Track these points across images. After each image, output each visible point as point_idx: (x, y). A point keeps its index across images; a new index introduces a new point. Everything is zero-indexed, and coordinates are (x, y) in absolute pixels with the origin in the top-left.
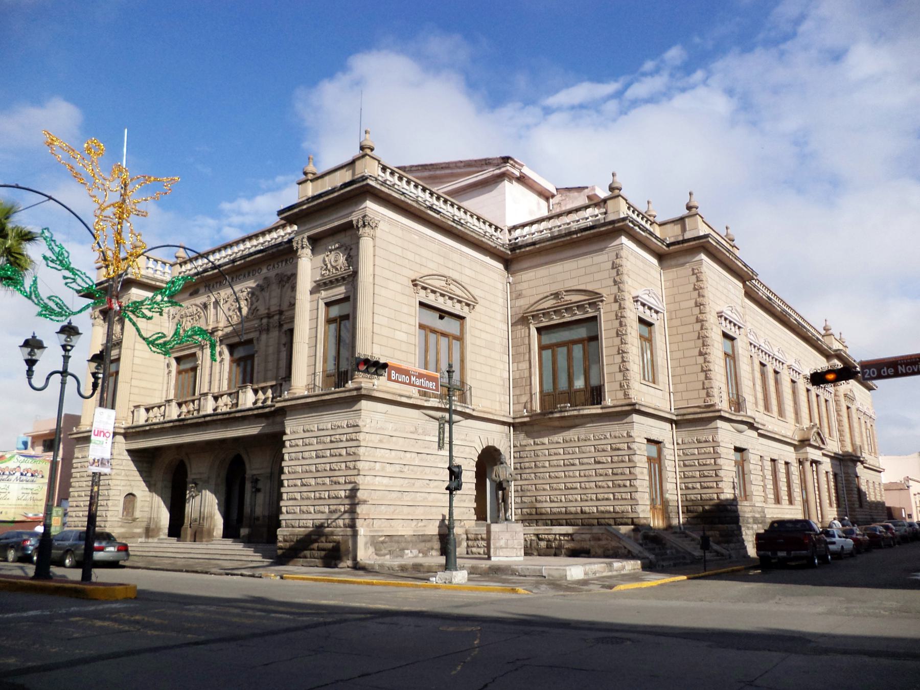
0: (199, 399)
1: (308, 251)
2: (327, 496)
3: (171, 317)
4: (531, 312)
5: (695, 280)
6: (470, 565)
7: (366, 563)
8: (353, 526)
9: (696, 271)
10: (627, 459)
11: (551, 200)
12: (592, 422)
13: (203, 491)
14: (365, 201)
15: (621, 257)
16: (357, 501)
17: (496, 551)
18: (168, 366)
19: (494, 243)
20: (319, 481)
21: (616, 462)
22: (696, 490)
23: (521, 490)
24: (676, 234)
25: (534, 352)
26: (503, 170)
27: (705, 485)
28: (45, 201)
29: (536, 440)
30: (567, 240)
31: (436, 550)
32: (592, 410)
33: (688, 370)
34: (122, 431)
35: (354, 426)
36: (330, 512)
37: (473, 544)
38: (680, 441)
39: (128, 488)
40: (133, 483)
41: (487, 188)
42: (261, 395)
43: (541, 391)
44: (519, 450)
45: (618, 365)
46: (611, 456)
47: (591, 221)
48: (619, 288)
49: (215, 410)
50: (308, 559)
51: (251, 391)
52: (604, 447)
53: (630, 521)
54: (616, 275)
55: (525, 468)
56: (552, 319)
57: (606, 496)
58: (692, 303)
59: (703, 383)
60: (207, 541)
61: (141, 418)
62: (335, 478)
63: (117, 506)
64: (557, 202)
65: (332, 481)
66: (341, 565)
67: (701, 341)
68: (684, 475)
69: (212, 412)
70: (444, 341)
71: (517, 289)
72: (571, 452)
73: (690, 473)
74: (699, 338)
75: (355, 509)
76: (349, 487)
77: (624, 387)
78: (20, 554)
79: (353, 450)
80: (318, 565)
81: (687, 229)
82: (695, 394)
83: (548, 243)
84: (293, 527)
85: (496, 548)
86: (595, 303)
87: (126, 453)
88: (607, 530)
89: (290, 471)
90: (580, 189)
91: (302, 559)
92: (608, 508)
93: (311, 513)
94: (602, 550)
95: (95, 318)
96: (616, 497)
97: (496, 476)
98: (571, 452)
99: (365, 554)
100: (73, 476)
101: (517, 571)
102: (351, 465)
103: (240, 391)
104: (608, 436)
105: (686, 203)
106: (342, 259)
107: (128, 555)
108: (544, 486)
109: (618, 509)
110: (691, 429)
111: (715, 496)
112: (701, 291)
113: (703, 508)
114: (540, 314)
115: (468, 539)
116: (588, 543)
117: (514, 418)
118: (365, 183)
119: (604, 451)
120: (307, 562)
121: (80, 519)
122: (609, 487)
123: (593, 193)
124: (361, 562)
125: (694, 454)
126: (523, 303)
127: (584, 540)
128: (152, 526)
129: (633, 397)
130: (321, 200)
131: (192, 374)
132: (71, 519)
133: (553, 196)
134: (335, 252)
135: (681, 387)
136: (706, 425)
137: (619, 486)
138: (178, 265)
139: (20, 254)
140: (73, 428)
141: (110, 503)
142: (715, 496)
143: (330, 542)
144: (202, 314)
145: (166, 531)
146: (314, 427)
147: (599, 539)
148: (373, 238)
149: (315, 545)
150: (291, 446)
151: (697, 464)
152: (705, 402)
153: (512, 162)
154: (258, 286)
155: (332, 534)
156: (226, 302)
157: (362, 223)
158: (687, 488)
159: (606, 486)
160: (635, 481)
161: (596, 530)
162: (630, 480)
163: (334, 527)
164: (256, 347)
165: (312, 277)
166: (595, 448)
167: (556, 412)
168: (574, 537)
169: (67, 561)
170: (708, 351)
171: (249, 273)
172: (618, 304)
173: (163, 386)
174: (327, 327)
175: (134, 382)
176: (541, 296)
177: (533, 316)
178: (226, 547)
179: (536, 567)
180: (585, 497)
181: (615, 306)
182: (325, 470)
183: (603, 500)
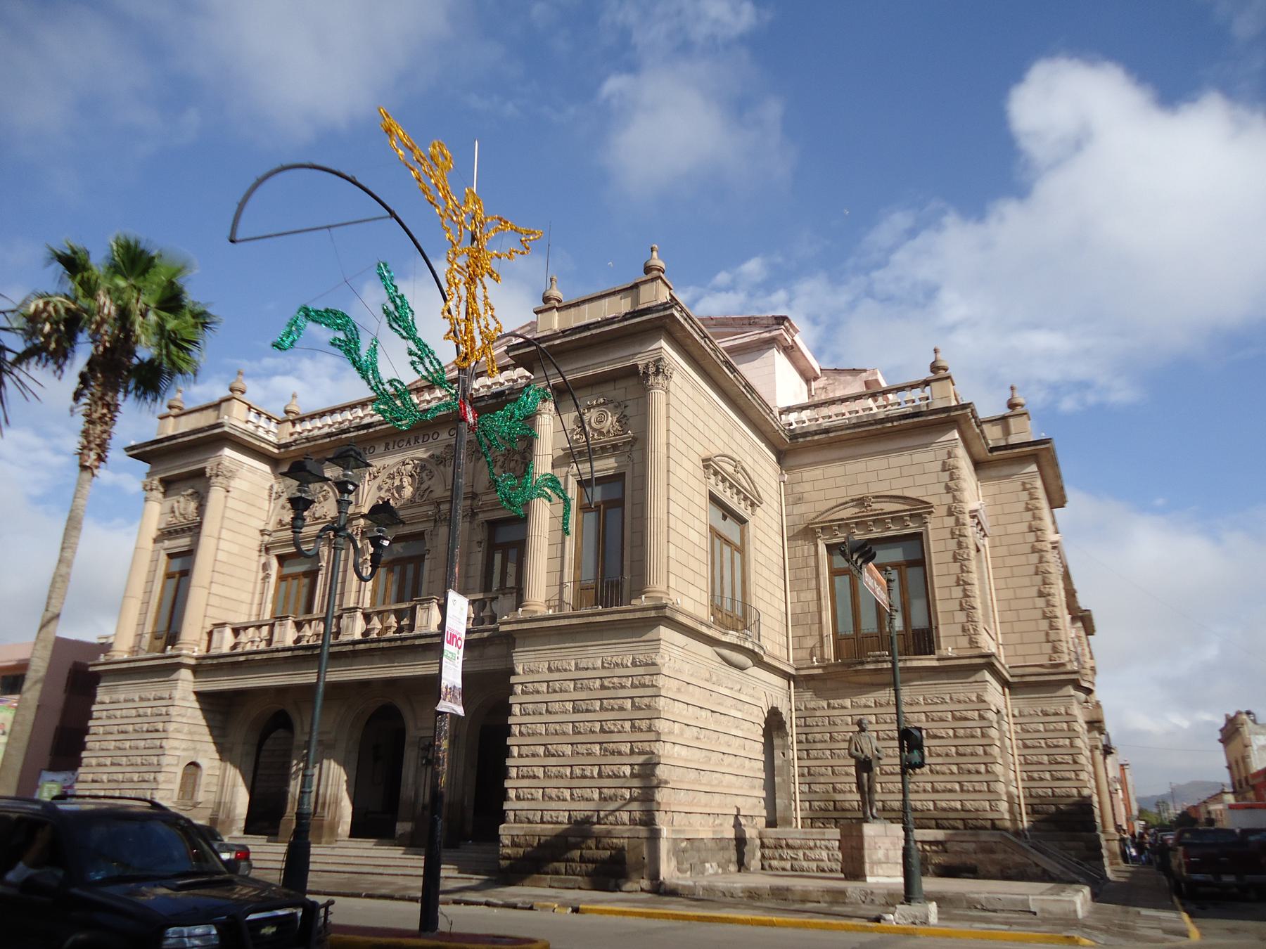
0: (272, 626)
2: (595, 774)
3: (274, 495)
4: (822, 522)
6: (886, 891)
7: (677, 885)
8: (648, 821)
11: (812, 383)
12: (921, 679)
13: (325, 762)
15: (956, 457)
16: (655, 782)
18: (265, 567)
19: (777, 425)
20: (582, 749)
21: (962, 737)
23: (809, 774)
25: (825, 578)
27: (1059, 775)
29: (832, 701)
31: (733, 862)
32: (923, 662)
33: (1023, 615)
34: (193, 662)
35: (647, 665)
36: (603, 799)
38: (1016, 713)
39: (191, 753)
40: (199, 746)
41: (747, 357)
42: (376, 623)
44: (805, 716)
47: (848, 419)
48: (954, 497)
49: (234, 647)
50: (562, 877)
53: (988, 824)
54: (948, 479)
55: (814, 742)
57: (949, 786)
58: (1024, 527)
59: (1047, 634)
60: (327, 843)
61: (225, 642)
63: (171, 782)
64: (821, 386)
65: (606, 750)
67: (1039, 578)
68: (1025, 759)
69: (361, 638)
76: (641, 759)
77: (969, 631)
79: (646, 701)
82: (1035, 649)
83: (848, 432)
84: (530, 822)
85: (873, 863)
86: (919, 515)
87: (193, 697)
88: (1002, 836)
89: (525, 732)
90: (855, 372)
91: (549, 876)
93: (564, 800)
95: (151, 490)
97: (857, 750)
99: (668, 870)
100: (91, 732)
104: (948, 699)
106: (192, 505)
109: (968, 805)
111: (1075, 791)
113: (1058, 808)
114: (835, 525)
115: (763, 846)
116: (974, 856)
117: (796, 669)
118: (668, 312)
122: (952, 773)
123: (874, 378)
124: (667, 882)
125: (1039, 731)
126: (807, 511)
127: (966, 852)
128: (222, 816)
131: (306, 581)
133: (816, 378)
134: (597, 409)
135: (1014, 638)
137: (969, 772)
138: (290, 423)
140: (99, 655)
142: (1075, 791)
143: (605, 849)
144: (331, 494)
145: (242, 824)
146: (569, 664)
147: (992, 851)
148: (667, 391)
149: (576, 854)
150: (524, 692)
151: (1044, 745)
152: (1051, 660)
153: (787, 324)
154: (432, 456)
155: (609, 834)
157: (654, 369)
159: (947, 771)
160: (992, 766)
161: (985, 836)
163: (611, 824)
164: (427, 545)
166: (927, 716)
168: (948, 845)
170: (1052, 591)
171: (416, 441)
174: (580, 516)
175: (215, 589)
176: (834, 503)
177: (822, 528)
178: (366, 853)
180: (915, 787)
181: (951, 521)
182: (592, 732)
183: (944, 791)
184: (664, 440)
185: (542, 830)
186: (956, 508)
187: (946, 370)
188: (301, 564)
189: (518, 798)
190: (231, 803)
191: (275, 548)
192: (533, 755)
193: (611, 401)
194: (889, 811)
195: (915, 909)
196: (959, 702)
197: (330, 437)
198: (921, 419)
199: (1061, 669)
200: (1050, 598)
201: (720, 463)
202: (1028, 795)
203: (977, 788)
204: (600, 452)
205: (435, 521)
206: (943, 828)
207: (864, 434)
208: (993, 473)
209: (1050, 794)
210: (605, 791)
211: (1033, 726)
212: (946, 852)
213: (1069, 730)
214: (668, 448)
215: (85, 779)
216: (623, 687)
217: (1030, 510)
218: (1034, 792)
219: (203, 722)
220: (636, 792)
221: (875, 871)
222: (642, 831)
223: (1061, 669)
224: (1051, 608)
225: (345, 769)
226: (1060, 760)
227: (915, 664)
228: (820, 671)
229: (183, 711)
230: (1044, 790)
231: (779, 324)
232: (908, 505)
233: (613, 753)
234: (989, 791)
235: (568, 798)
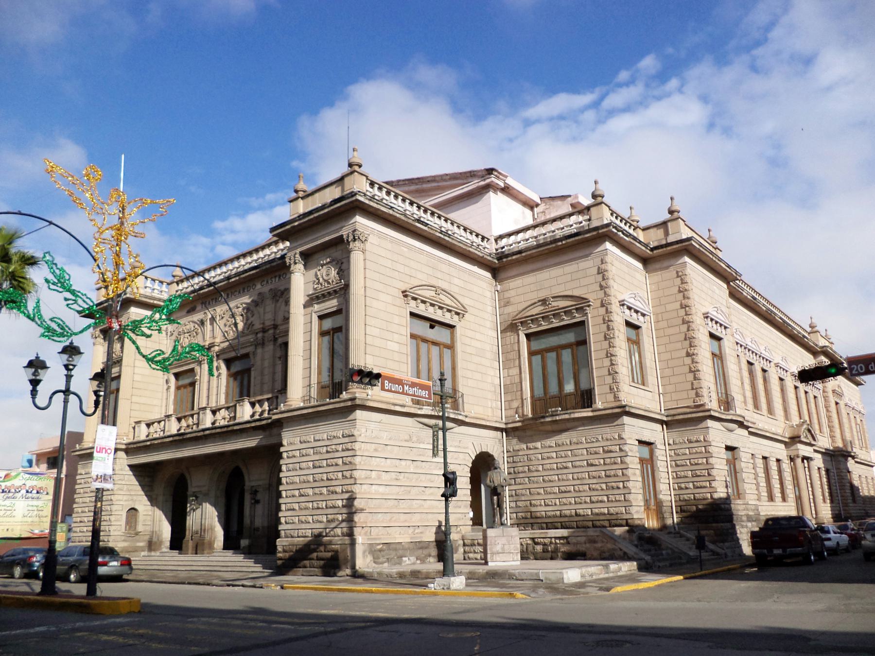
0: (198, 414)
3: (169, 334)
7: (364, 571)
8: (351, 534)
9: (680, 274)
12: (584, 425)
13: (204, 504)
15: (606, 262)
16: (354, 510)
17: (493, 556)
18: (167, 382)
19: (482, 253)
21: (609, 464)
23: (516, 495)
25: (524, 358)
26: (488, 181)
27: (698, 484)
29: (529, 444)
30: (552, 247)
33: (677, 371)
34: (124, 447)
35: (349, 436)
36: (328, 521)
37: (470, 550)
38: (671, 442)
39: (130, 503)
40: (135, 498)
41: (473, 200)
42: (258, 408)
43: (532, 397)
44: (512, 455)
45: (607, 368)
46: (603, 459)
48: (605, 293)
49: (213, 423)
50: (308, 569)
51: (248, 404)
53: (624, 522)
54: (601, 280)
55: (519, 473)
57: (600, 498)
58: (678, 305)
59: (692, 384)
61: (142, 433)
62: (332, 488)
64: (542, 210)
65: (329, 491)
66: (340, 573)
67: (688, 342)
68: (676, 475)
69: (211, 426)
70: (435, 350)
72: (564, 456)
73: (683, 473)
74: (685, 339)
75: (353, 518)
76: (346, 496)
77: (614, 390)
79: (349, 459)
81: (670, 233)
82: (684, 395)
83: (534, 251)
84: (292, 537)
85: (493, 554)
86: (582, 308)
87: (128, 468)
89: (288, 482)
90: (563, 198)
91: (301, 569)
95: (96, 338)
96: (610, 499)
97: (490, 482)
99: (363, 562)
101: (514, 575)
102: (348, 474)
103: (238, 405)
106: (333, 272)
107: (131, 569)
108: (538, 490)
109: (612, 510)
111: (709, 496)
112: (686, 293)
115: (464, 545)
118: (354, 198)
119: (596, 453)
122: (602, 490)
123: (576, 201)
124: (360, 570)
126: (512, 310)
128: (155, 539)
130: (312, 217)
133: (537, 205)
134: (327, 266)
135: (670, 388)
137: (613, 488)
138: (175, 284)
142: (709, 496)
143: (328, 551)
144: (200, 330)
145: (168, 544)
146: (310, 437)
147: (595, 542)
149: (315, 555)
150: (288, 457)
151: (689, 464)
152: (694, 403)
153: (496, 173)
154: (252, 301)
155: (330, 543)
156: (222, 318)
157: (352, 237)
159: (599, 488)
160: (628, 483)
161: (591, 532)
162: (623, 482)
163: (332, 536)
166: (587, 451)
167: (547, 416)
169: (72, 576)
170: (696, 351)
171: (244, 291)
174: (320, 339)
176: (529, 303)
177: (521, 323)
180: (579, 500)
181: (602, 311)
183: (597, 502)
184: (362, 284)
185: (298, 541)
186: (605, 301)
187: (603, 197)
188: (188, 378)
189: (286, 523)
190: (159, 531)
191: (172, 369)
194: (564, 517)
196: (607, 440)
197: (239, 275)
198: (580, 237)
199: (701, 409)
200: (694, 357)
201: (416, 292)
202: (678, 499)
203: (617, 499)
204: (328, 296)
205: (256, 346)
206: (567, 528)
207: (546, 251)
208: (657, 266)
209: (692, 498)
210: (329, 516)
211: (681, 451)
212: (569, 544)
213: (706, 452)
215: (76, 521)
216: (337, 451)
219: (137, 483)
220: (345, 516)
221: (495, 559)
222: (347, 540)
224: (694, 365)
225: (215, 508)
227: (577, 415)
229: (122, 477)
230: (688, 495)
232: (576, 301)
233: (332, 493)
234: (625, 500)
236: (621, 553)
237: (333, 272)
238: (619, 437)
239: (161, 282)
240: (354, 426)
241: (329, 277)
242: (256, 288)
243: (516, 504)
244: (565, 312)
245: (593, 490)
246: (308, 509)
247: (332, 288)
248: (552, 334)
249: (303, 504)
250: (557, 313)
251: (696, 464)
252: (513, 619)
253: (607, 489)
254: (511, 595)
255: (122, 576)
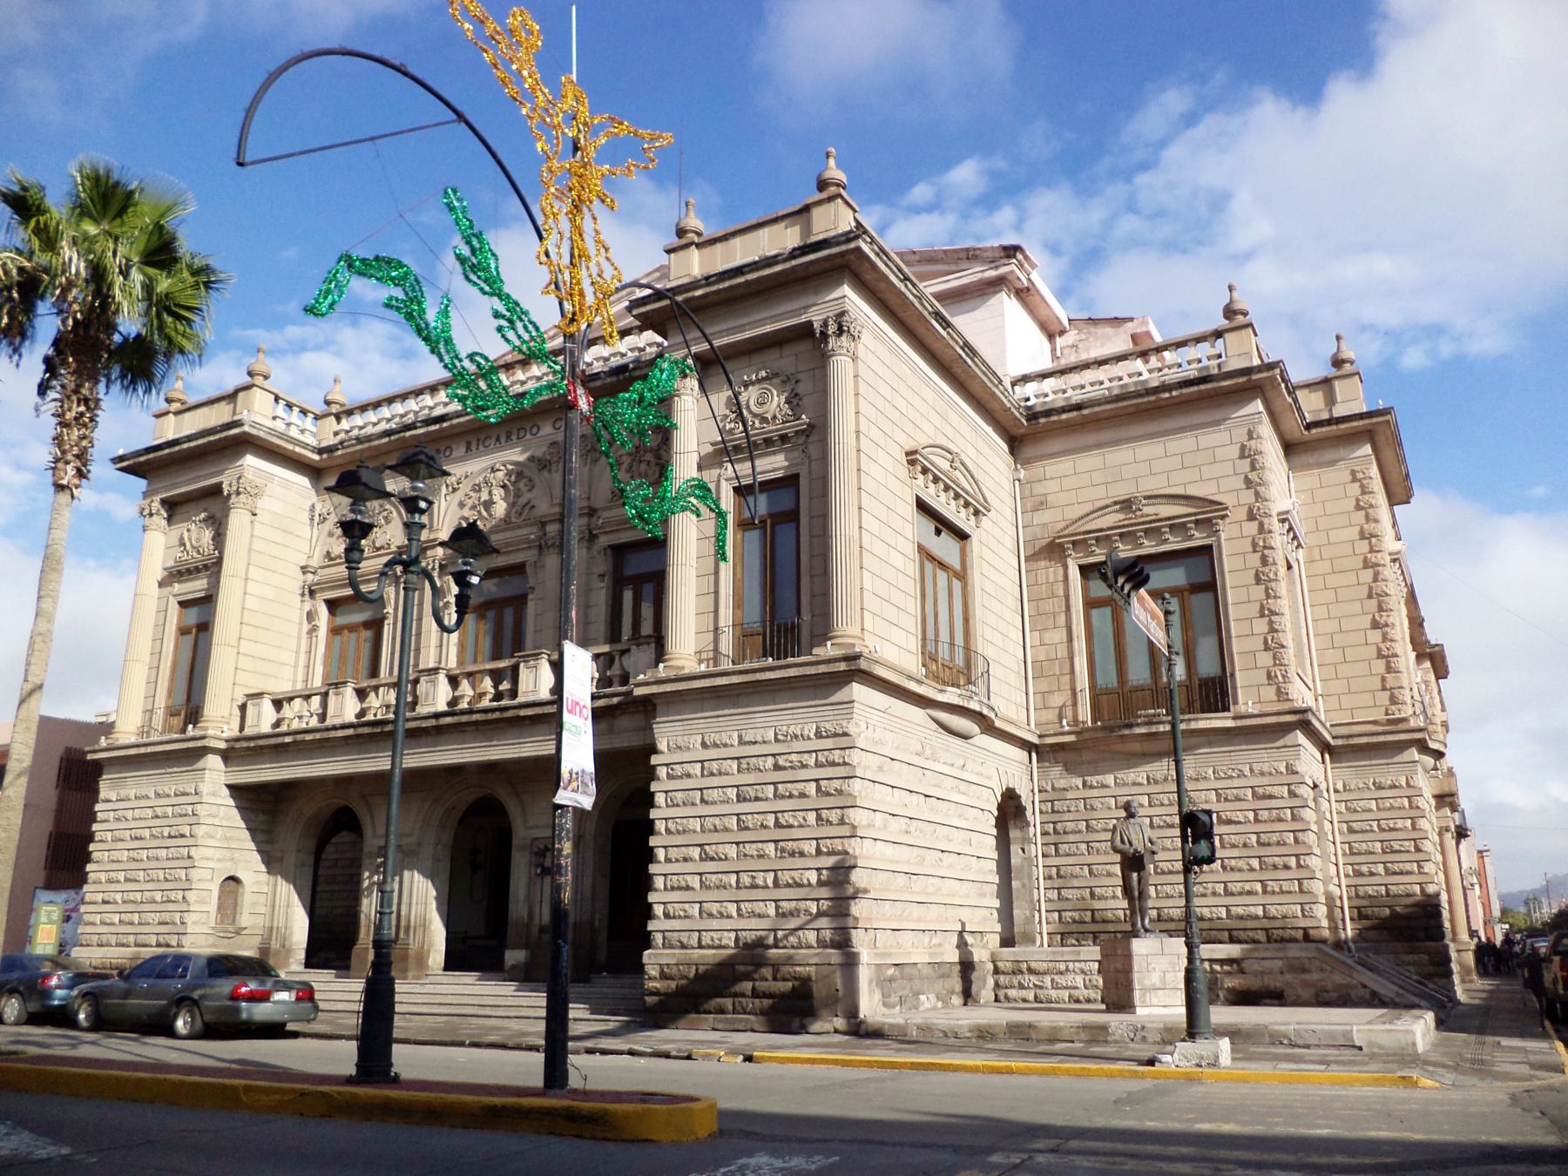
0: (325, 695)
1: (692, 383)
3: (317, 518)
4: (1073, 535)
5: (1359, 491)
7: (885, 1024)
8: (842, 942)
9: (1360, 475)
10: (1289, 816)
11: (1058, 339)
12: (1210, 745)
13: (406, 874)
14: (839, 284)
15: (1259, 437)
16: (850, 891)
17: (1144, 995)
18: (310, 616)
22: (1377, 878)
23: (1059, 876)
24: (1314, 408)
25: (1078, 611)
26: (1003, 270)
27: (1396, 867)
28: (448, 122)
29: (1088, 779)
30: (1149, 402)
34: (222, 745)
35: (836, 735)
36: (781, 915)
37: (1011, 981)
38: (1340, 787)
39: (228, 864)
40: (237, 855)
41: (965, 305)
42: (466, 688)
43: (1093, 686)
44: (1052, 798)
45: (1262, 638)
46: (1254, 810)
48: (1257, 494)
49: (277, 724)
51: (547, 664)
52: (1241, 792)
54: (1248, 469)
55: (1065, 833)
56: (1092, 553)
57: (1247, 887)
58: (1354, 533)
59: (1383, 679)
61: (263, 720)
62: (790, 843)
64: (1070, 343)
65: (783, 850)
66: (817, 1026)
67: (1374, 602)
68: (1351, 848)
70: (942, 576)
71: (1035, 492)
72: (1167, 802)
73: (1364, 845)
74: (1370, 596)
75: (848, 908)
76: (830, 861)
77: (1275, 679)
78: (33, 1007)
79: (836, 784)
80: (756, 1027)
81: (1339, 400)
82: (1367, 699)
84: (683, 946)
85: (1144, 990)
86: (1209, 520)
87: (226, 792)
88: (1318, 949)
90: (1117, 321)
92: (1252, 909)
94: (1312, 991)
95: (151, 515)
96: (1269, 889)
97: (1122, 842)
98: (1167, 802)
99: (870, 1006)
101: (1285, 1036)
102: (834, 816)
103: (522, 665)
104: (1247, 773)
105: (1331, 354)
106: (207, 535)
107: (316, 1009)
108: (1108, 867)
109: (1273, 911)
110: (1362, 763)
111: (1417, 889)
112: (1371, 511)
114: (1091, 539)
115: (996, 971)
117: (1040, 736)
118: (852, 245)
119: (1238, 799)
120: (727, 1021)
121: (112, 929)
122: (1252, 869)
123: (1144, 329)
124: (870, 1020)
125: (1370, 810)
129: (1295, 697)
130: (741, 280)
132: (89, 929)
133: (1062, 332)
134: (757, 386)
136: (1393, 757)
137: (1275, 867)
139: (189, 309)
140: (99, 739)
141: (191, 896)
142: (1417, 889)
143: (785, 980)
144: (395, 513)
145: (302, 955)
146: (730, 737)
147: (1304, 970)
148: (854, 359)
149: (747, 986)
150: (670, 777)
151: (1376, 828)
152: (1387, 714)
153: (1020, 256)
154: (531, 459)
155: (789, 961)
156: (454, 490)
158: (1359, 874)
160: (1307, 858)
161: (1294, 951)
162: (1297, 856)
163: (793, 947)
165: (164, 562)
167: (1138, 725)
169: (180, 1023)
170: (1390, 620)
171: (508, 437)
172: (1255, 524)
173: (297, 658)
174: (739, 536)
176: (1088, 508)
177: (1074, 543)
179: (1333, 1027)
181: (1252, 528)
183: (1240, 894)
184: (852, 427)
187: (1245, 314)
188: (360, 611)
191: (322, 590)
192: (685, 860)
193: (776, 375)
195: (1201, 1047)
196: (1262, 774)
198: (1210, 386)
199: (1402, 726)
203: (1284, 889)
206: (1239, 942)
207: (1131, 410)
208: (1311, 458)
214: (858, 438)
215: (94, 899)
216: (804, 766)
217: (1363, 508)
218: (1361, 891)
222: (834, 956)
223: (1402, 726)
226: (1397, 847)
227: (1202, 724)
228: (1072, 738)
231: (1009, 257)
234: (1301, 891)
235: (735, 914)
236: (1366, 994)
237: (776, 398)
238: (1287, 767)
239: (304, 412)
240: (849, 716)
241: (765, 408)
242: (540, 434)
243: (1059, 894)
244: (1171, 527)
245: (1232, 869)
246: (725, 888)
247: (777, 430)
248: (1173, 563)
249: (714, 877)
250: (1129, 533)
251: (1391, 830)
252: (926, 1113)
253: (1261, 868)
254: (1407, 1082)
255: (284, 1024)
